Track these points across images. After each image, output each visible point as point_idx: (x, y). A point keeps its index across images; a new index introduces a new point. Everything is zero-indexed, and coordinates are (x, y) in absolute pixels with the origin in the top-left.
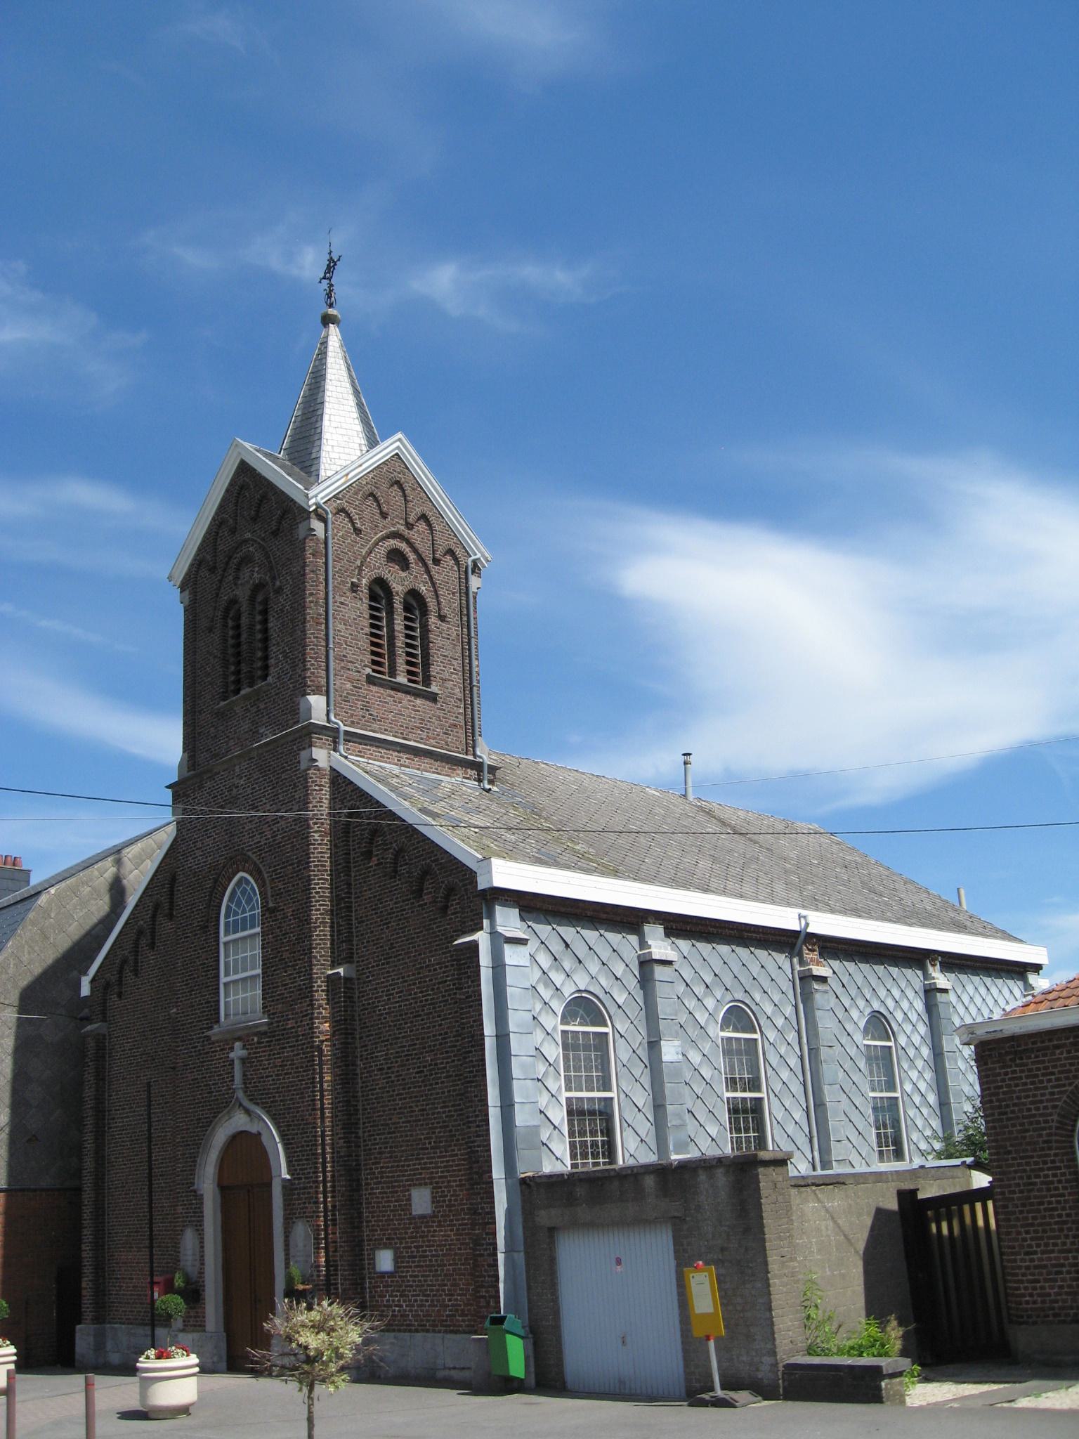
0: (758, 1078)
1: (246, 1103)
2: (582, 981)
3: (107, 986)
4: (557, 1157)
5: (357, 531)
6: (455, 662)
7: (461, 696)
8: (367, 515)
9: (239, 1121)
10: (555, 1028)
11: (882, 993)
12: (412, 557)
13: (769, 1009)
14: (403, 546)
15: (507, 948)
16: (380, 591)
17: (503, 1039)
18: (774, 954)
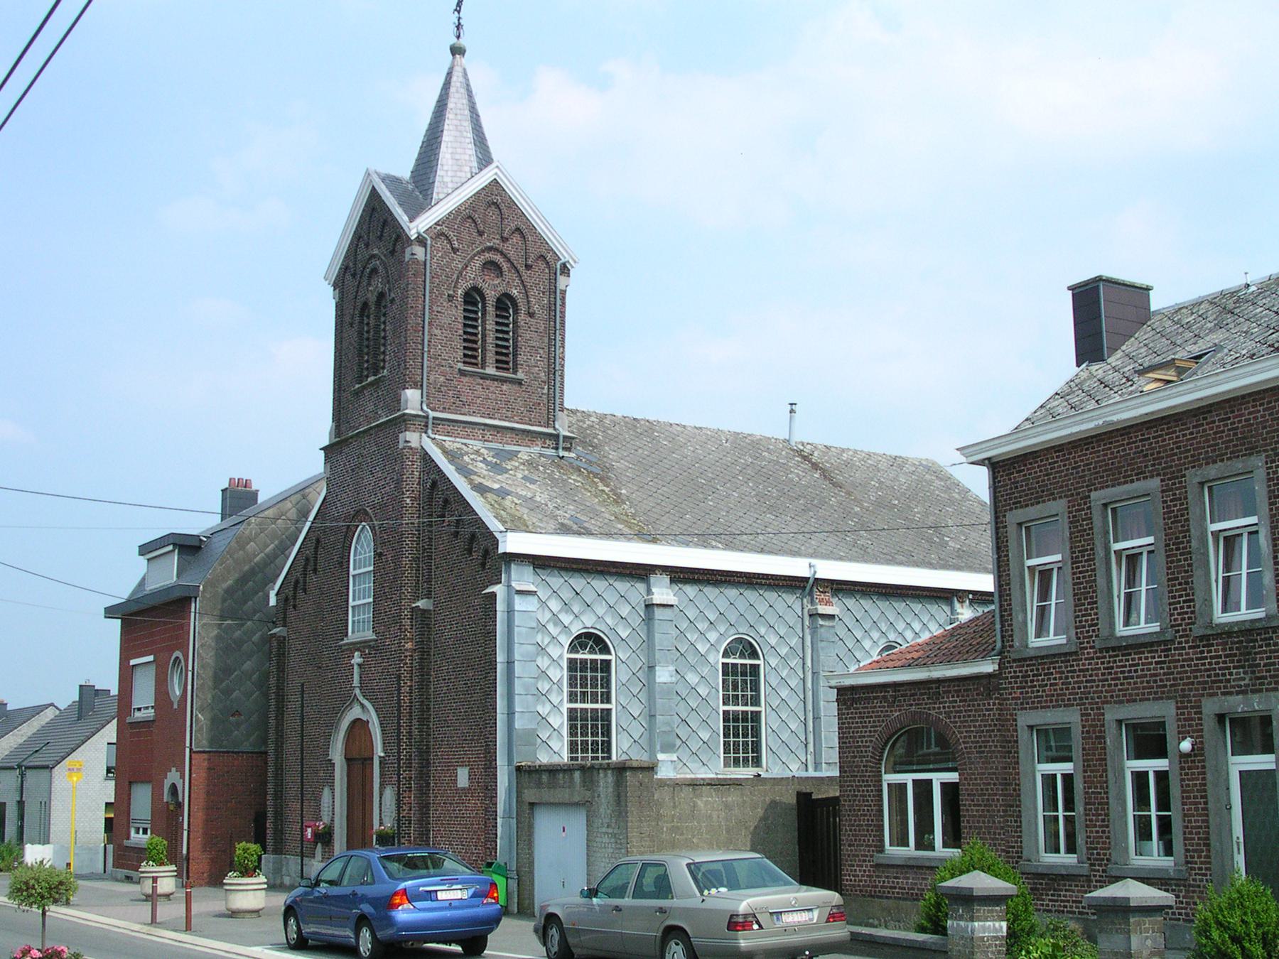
0: (759, 695)
1: (361, 698)
3: (287, 599)
4: (556, 750)
5: (455, 250)
6: (541, 351)
7: (545, 378)
8: (465, 235)
9: (355, 713)
10: (561, 656)
11: (901, 626)
12: (505, 266)
13: (773, 640)
14: (498, 258)
15: (517, 599)
17: (510, 663)
18: (784, 595)
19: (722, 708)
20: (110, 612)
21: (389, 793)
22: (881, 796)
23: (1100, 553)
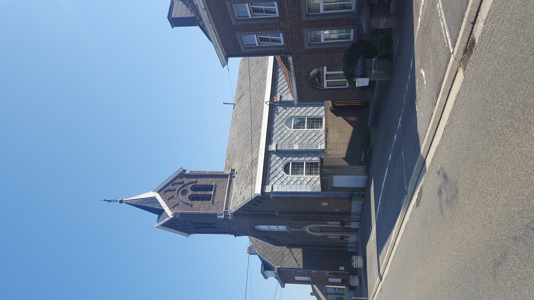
2: (280, 169)
16: (193, 198)
19: (306, 129)
20: (283, 286)
21: (329, 223)
22: (331, 89)
23: (252, 22)
